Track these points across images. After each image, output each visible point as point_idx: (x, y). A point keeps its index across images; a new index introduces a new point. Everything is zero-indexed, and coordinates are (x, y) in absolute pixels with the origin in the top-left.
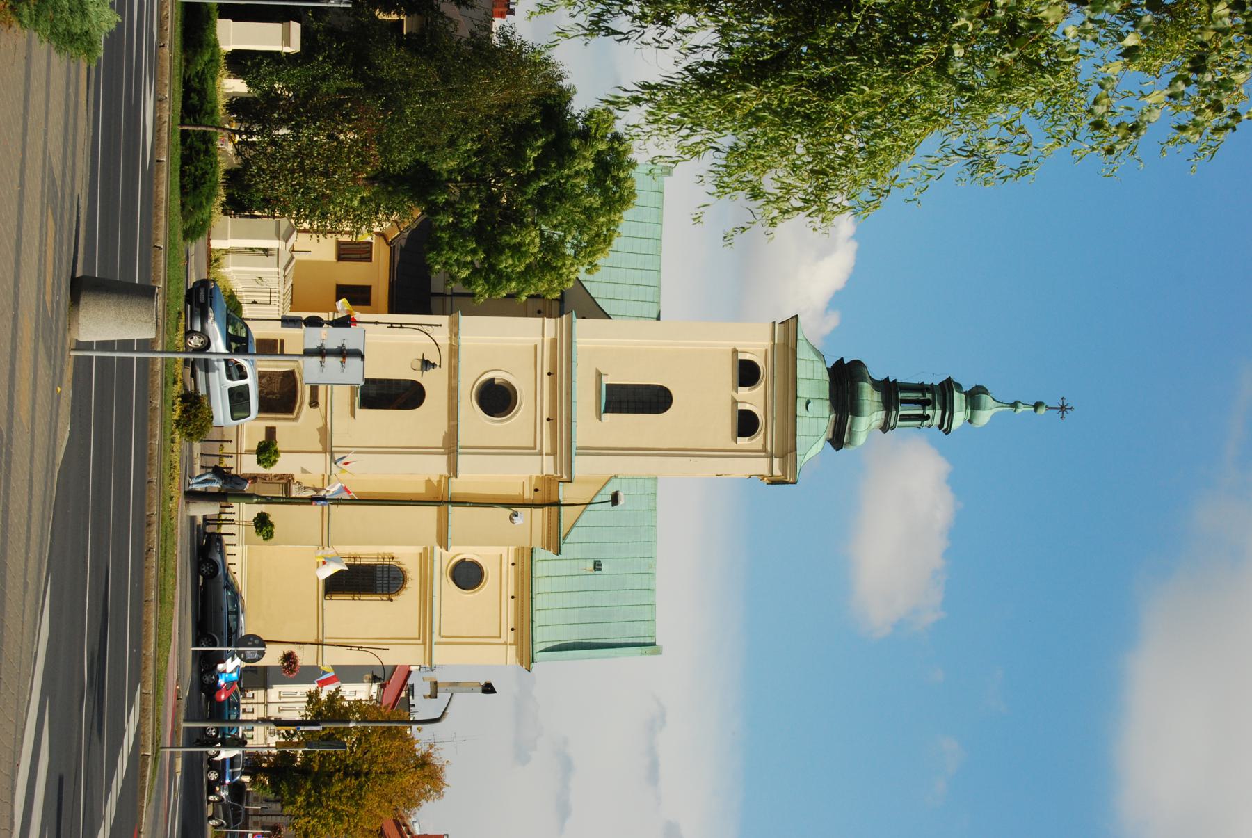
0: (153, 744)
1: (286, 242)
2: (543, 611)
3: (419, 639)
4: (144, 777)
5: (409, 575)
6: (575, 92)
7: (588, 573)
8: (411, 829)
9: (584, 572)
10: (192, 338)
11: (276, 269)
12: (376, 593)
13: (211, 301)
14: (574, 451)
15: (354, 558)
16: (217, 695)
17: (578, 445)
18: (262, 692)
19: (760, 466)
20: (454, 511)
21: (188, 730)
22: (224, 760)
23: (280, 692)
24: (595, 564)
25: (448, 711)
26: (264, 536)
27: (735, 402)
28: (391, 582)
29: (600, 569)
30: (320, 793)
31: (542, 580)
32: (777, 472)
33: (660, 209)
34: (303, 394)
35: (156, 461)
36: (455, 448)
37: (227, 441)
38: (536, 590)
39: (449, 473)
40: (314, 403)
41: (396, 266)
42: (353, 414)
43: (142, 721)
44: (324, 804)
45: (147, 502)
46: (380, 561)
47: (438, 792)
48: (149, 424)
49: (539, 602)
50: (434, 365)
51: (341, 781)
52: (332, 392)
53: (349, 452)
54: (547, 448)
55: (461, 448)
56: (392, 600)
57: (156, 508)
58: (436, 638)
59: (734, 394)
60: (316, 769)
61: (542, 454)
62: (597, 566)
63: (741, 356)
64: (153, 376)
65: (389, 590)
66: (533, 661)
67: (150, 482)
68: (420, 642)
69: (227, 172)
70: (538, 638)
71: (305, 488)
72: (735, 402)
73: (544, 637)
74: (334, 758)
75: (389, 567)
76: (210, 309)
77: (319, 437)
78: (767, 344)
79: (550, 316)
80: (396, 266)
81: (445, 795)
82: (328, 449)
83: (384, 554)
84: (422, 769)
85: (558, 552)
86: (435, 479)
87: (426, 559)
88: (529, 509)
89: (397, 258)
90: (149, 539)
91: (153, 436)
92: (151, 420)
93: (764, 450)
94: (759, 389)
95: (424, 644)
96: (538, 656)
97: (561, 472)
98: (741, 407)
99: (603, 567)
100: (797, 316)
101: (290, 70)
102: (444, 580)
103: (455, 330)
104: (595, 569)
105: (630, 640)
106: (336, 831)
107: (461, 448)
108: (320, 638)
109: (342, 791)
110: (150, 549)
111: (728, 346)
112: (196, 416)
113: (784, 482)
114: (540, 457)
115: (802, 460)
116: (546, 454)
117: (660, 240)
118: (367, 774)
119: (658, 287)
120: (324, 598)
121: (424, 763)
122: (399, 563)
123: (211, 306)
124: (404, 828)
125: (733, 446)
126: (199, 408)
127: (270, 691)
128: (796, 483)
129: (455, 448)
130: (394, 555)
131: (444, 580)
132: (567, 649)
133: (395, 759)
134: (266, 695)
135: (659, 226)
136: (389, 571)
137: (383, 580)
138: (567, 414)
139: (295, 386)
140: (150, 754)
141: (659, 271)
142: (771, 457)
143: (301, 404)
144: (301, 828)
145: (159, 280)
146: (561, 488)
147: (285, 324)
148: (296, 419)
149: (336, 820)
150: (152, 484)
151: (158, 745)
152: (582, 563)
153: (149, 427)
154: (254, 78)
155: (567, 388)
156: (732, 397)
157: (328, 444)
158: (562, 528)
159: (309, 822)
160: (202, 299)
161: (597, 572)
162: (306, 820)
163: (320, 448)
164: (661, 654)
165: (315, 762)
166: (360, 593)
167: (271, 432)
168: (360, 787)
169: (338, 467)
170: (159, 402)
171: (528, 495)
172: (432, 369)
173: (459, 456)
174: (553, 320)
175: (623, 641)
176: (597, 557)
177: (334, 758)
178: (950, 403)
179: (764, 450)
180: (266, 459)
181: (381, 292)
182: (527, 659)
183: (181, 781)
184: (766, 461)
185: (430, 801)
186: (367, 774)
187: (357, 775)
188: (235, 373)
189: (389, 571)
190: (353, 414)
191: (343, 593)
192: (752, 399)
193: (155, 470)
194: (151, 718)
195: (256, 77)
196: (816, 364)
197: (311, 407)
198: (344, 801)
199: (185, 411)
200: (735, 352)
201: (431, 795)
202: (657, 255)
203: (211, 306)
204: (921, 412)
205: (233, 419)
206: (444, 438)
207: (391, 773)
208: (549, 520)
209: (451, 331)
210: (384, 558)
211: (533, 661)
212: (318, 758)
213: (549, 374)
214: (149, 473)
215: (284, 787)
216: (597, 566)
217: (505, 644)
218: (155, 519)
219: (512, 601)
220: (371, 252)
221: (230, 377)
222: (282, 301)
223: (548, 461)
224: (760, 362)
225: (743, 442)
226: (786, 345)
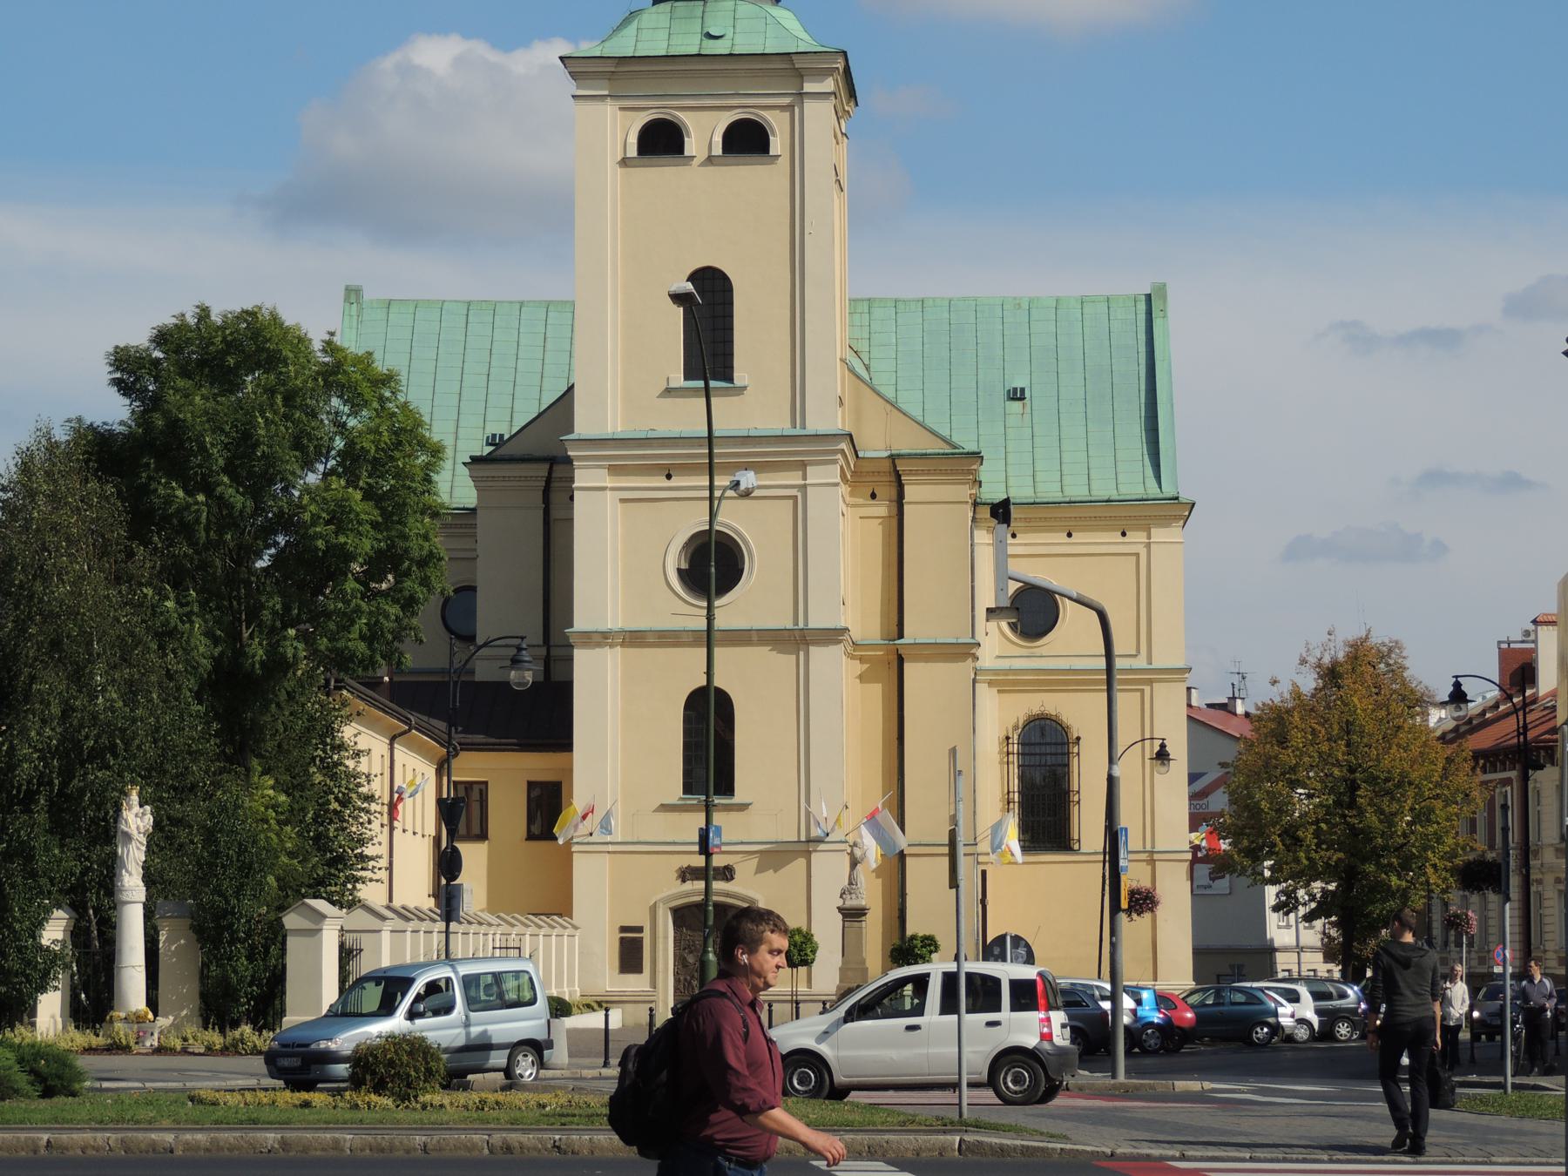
0: (945, 1132)
1: (324, 917)
2: (1092, 483)
3: (1142, 691)
4: (1003, 1150)
5: (1036, 710)
6: (79, 420)
7: (1028, 410)
8: (1491, 703)
9: (1027, 417)
10: (522, 1076)
11: (408, 934)
12: (1068, 765)
13: (299, 1046)
14: (798, 431)
15: (1009, 803)
16: (1186, 1025)
17: (788, 425)
18: (1280, 957)
19: (819, 116)
20: (915, 631)
21: (1128, 1072)
22: (1318, 1012)
23: (1279, 927)
24: (1013, 399)
25: (1075, 595)
26: (931, 952)
27: (710, 160)
28: (1048, 740)
29: (1023, 390)
30: (1384, 848)
31: (1040, 487)
32: (828, 85)
33: (416, 304)
35: (384, 1139)
36: (797, 633)
37: (651, 1016)
38: (1058, 497)
39: (840, 642)
41: (498, 741)
42: (743, 807)
43: (891, 1155)
44: (1402, 841)
45: (463, 1153)
46: (1014, 759)
47: (1390, 650)
48: (313, 1153)
49: (1077, 491)
50: (1163, 746)
51: (1361, 813)
52: (742, 843)
53: (808, 814)
54: (794, 478)
55: (796, 622)
56: (1078, 739)
57: (476, 1137)
59: (696, 162)
60: (1341, 855)
61: (805, 486)
62: (1017, 395)
63: (633, 151)
64: (220, 1149)
65: (1063, 744)
67: (425, 1148)
68: (1147, 689)
70: (1138, 491)
71: (850, 883)
72: (710, 160)
73: (1134, 481)
74: (1323, 825)
75: (1022, 743)
76: (313, 1046)
78: (610, 109)
79: (572, 480)
80: (498, 741)
81: (1395, 638)
82: (803, 847)
83: (1000, 752)
84: (1340, 676)
85: (977, 456)
86: (858, 668)
87: (1007, 682)
88: (906, 508)
89: (479, 738)
90: (535, 1149)
91: (336, 1145)
92: (306, 1149)
93: (790, 108)
94: (687, 119)
95: (1150, 682)
96: (1168, 490)
97: (835, 452)
98: (718, 150)
99: (1019, 384)
100: (561, 58)
101: (14, 918)
102: (1037, 651)
103: (597, 638)
104: (1022, 398)
105: (1142, 337)
106: (1448, 819)
107: (796, 622)
108: (1144, 856)
109: (1380, 811)
110: (556, 1147)
111: (614, 175)
112: (391, 1063)
113: (847, 70)
114: (808, 488)
115: (806, 42)
116: (805, 478)
117: (469, 303)
118: (1352, 770)
119: (548, 305)
120: (1077, 852)
121: (1331, 675)
122: (1016, 727)
123: (307, 1045)
124: (1488, 715)
125: (784, 162)
126: (376, 1057)
127: (1277, 944)
128: (845, 53)
129: (797, 633)
130: (1004, 734)
131: (1043, 651)
132: (1157, 442)
133: (1325, 721)
134: (1286, 949)
135: (446, 304)
136: (1028, 744)
137: (1046, 754)
138: (735, 446)
140: (958, 1138)
141: (522, 304)
142: (801, 95)
143: (728, 895)
144: (1445, 879)
145: (33, 1140)
146: (869, 454)
147: (454, 915)
149: (1429, 820)
150: (430, 1146)
151: (952, 1123)
152: (1011, 421)
153: (318, 1153)
154: (28, 981)
155: (692, 446)
156: (702, 165)
157: (791, 847)
158: (937, 451)
159: (1434, 866)
160: (295, 1062)
161: (1027, 394)
162: (1430, 870)
163: (802, 862)
164: (1165, 285)
165: (1330, 858)
166: (1068, 792)
168: (1372, 780)
169: (833, 829)
170: (271, 1136)
171: (881, 509)
172: (1167, 749)
173: (810, 626)
174: (577, 473)
175: (1143, 349)
176: (1001, 394)
177: (1323, 825)
179: (790, 108)
180: (800, 951)
181: (537, 765)
182: (1177, 510)
183: (1219, 1081)
184: (809, 106)
185: (1407, 663)
186: (1352, 770)
187: (1353, 787)
188: (435, 1000)
189: (1028, 744)
190: (743, 807)
191: (1068, 819)
193: (399, 1138)
194: (886, 1137)
195: (27, 976)
196: (643, 25)
197: (732, 878)
198: (1395, 806)
199: (379, 1088)
200: (625, 162)
201: (1396, 662)
202: (494, 307)
203: (307, 1045)
205: (533, 1002)
206: (780, 652)
207: (1348, 728)
208: (923, 472)
209: (599, 645)
210: (1008, 754)
211: (1177, 498)
212: (1323, 853)
213: (669, 477)
214: (408, 1152)
215: (1376, 910)
216: (1017, 395)
217: (1148, 545)
218: (497, 1138)
219: (1077, 537)
220: (471, 784)
221: (448, 1009)
222: (483, 929)
223: (815, 475)
225: (777, 145)
226: (611, 76)
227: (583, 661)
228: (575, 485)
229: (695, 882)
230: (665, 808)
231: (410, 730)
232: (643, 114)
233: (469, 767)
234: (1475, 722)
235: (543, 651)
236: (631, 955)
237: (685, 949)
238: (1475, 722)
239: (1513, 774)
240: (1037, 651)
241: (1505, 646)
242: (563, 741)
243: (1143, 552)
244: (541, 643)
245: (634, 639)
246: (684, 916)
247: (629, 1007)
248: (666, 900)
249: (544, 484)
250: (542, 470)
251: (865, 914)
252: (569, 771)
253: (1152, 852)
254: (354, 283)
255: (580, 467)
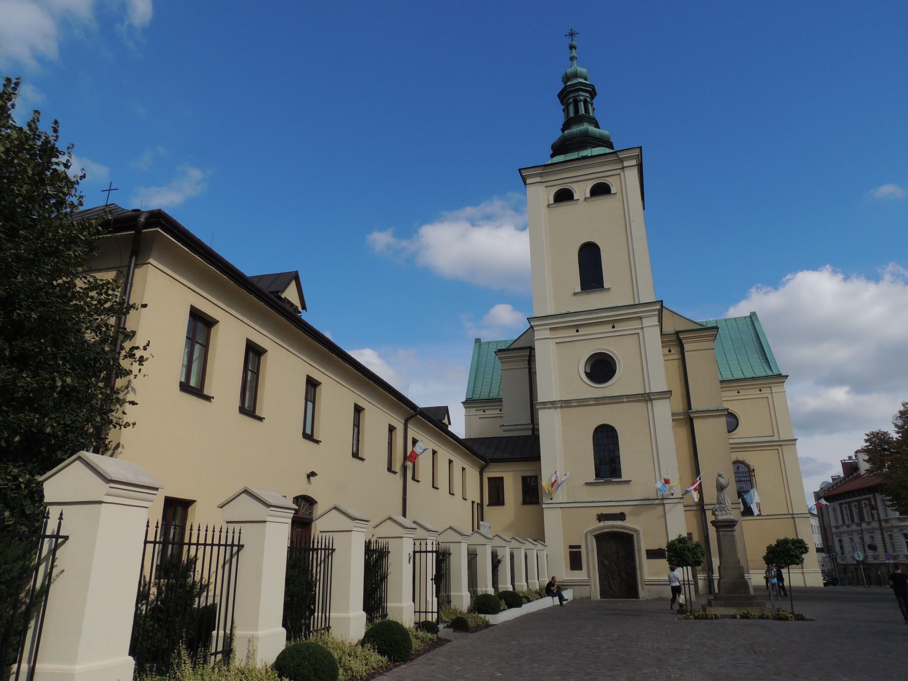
3: (778, 449)
26: (802, 553)
27: (586, 199)
34: (608, 527)
40: (621, 517)
52: (628, 501)
54: (636, 324)
56: (754, 470)
58: (776, 438)
61: (642, 328)
66: (781, 375)
68: (780, 448)
69: (867, 525)
73: (761, 371)
77: (677, 465)
88: (686, 354)
116: (642, 325)
139: (608, 534)
143: (623, 527)
148: (636, 531)
167: (653, 554)
178: (563, 93)
181: (525, 469)
190: (628, 482)
192: (581, 190)
200: (549, 206)
204: (582, 103)
223: (646, 322)
224: (554, 190)
227: (544, 417)
228: (535, 338)
229: (605, 522)
230: (587, 484)
231: (416, 415)
232: (555, 187)
233: (494, 472)
234: (839, 485)
235: (531, 426)
236: (575, 561)
237: (603, 557)
238: (839, 485)
239: (871, 496)
240: (732, 437)
241: (843, 462)
242: (537, 458)
243: (769, 396)
244: (530, 423)
245: (566, 404)
246: (602, 539)
247: (577, 588)
248: (591, 532)
249: (528, 358)
250: (527, 352)
251: (735, 525)
252: (539, 470)
253: (793, 514)
254: (478, 337)
255: (538, 330)
